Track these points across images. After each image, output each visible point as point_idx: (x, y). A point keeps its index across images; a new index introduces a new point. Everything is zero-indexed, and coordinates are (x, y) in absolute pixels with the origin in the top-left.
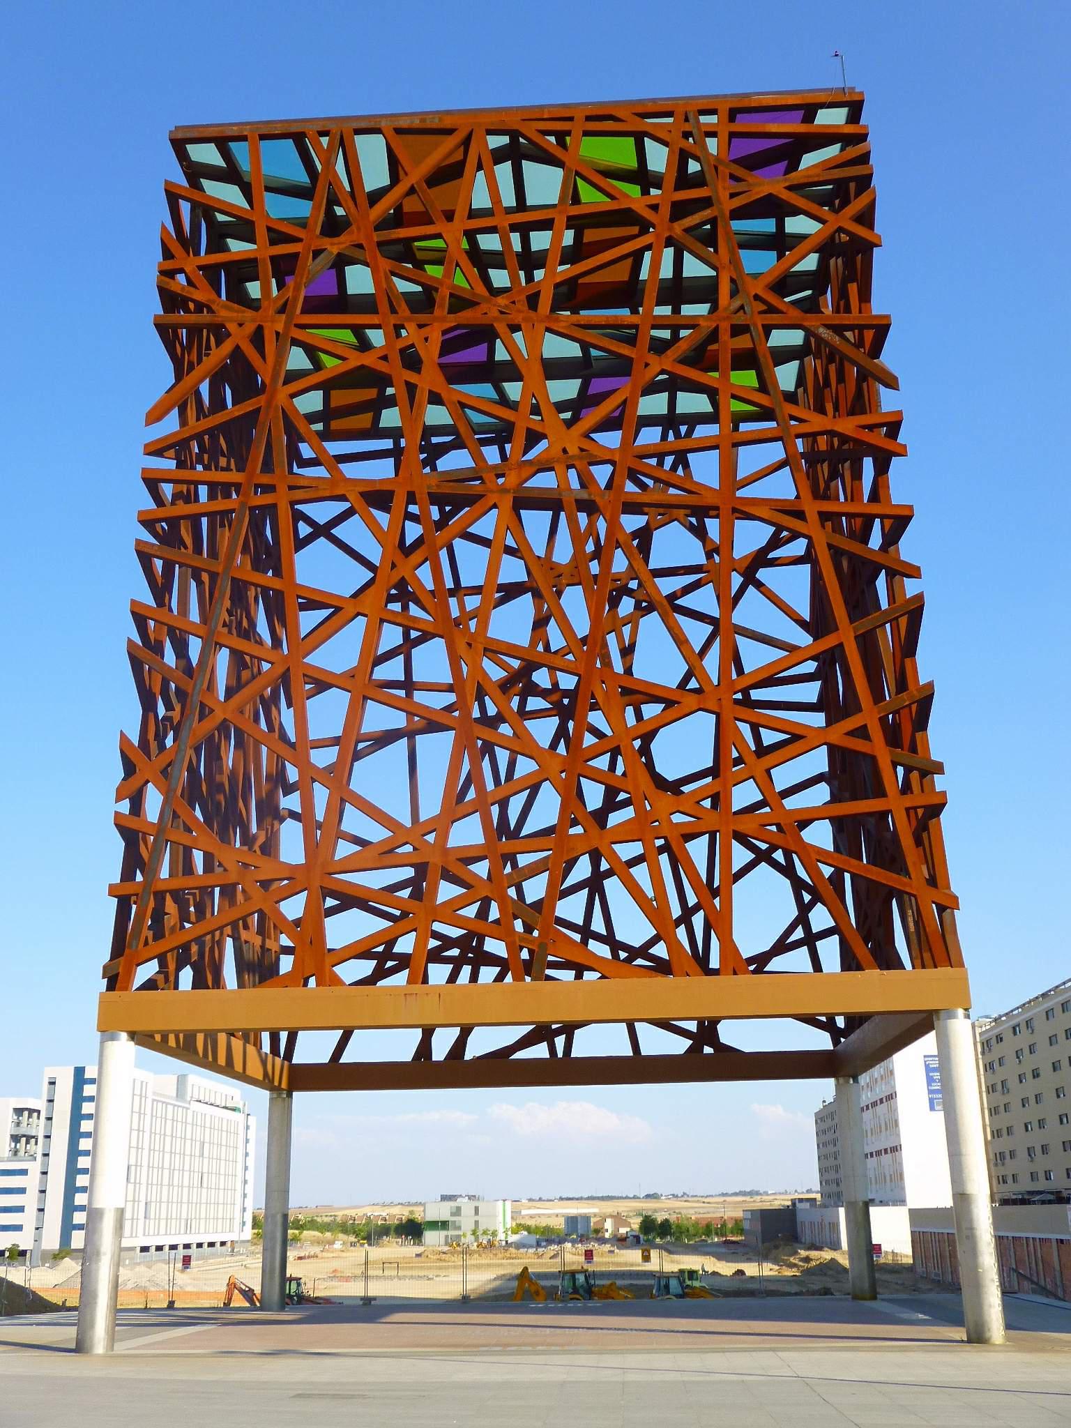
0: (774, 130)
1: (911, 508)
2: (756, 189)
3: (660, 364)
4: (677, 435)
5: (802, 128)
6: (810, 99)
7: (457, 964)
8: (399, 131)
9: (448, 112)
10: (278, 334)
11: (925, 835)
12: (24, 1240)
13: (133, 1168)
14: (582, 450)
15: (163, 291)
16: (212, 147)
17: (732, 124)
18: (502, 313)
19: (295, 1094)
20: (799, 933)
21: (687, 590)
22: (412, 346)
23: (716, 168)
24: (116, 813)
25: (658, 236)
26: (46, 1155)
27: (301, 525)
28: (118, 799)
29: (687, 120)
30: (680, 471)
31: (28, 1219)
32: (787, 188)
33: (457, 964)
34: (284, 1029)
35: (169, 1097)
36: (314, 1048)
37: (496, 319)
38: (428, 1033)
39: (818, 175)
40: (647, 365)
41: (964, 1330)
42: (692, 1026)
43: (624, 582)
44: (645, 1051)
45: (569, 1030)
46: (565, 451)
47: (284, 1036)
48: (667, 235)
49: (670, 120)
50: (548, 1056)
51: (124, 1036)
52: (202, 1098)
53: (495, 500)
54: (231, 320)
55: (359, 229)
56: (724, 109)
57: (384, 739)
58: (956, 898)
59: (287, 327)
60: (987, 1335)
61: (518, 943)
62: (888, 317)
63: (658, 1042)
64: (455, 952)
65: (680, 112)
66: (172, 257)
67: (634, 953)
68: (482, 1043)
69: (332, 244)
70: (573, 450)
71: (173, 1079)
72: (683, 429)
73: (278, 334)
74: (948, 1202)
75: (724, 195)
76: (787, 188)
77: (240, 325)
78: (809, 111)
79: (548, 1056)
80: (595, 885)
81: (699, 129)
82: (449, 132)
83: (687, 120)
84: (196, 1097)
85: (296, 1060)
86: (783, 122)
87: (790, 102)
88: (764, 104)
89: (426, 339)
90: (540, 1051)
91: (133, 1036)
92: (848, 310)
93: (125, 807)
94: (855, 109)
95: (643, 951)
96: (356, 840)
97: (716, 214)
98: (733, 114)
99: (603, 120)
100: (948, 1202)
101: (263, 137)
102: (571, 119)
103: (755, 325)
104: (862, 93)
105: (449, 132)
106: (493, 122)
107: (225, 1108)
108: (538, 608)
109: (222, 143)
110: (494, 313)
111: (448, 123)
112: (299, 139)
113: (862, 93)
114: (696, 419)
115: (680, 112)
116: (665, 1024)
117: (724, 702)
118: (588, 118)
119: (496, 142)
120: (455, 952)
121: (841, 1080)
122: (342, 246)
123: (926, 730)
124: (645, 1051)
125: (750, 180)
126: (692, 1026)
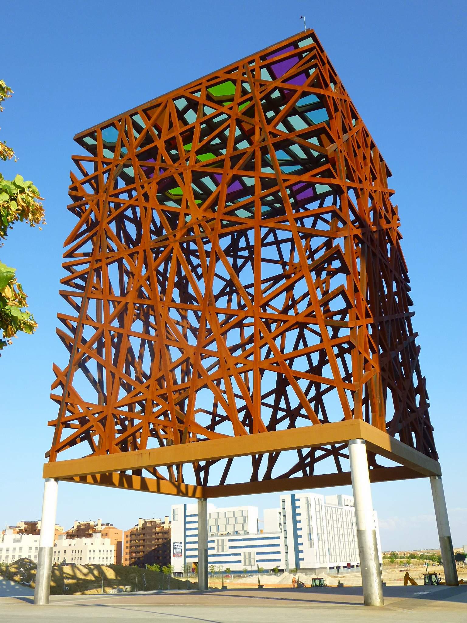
2: (269, 87)
9: (160, 97)
12: (282, 566)
13: (320, 535)
14: (204, 217)
19: (208, 499)
31: (282, 556)
32: (282, 82)
35: (336, 505)
37: (174, 173)
41: (362, 597)
46: (197, 219)
51: (52, 480)
52: (349, 504)
56: (257, 58)
59: (106, 198)
60: (369, 601)
70: (200, 218)
71: (336, 497)
76: (282, 82)
78: (295, 44)
82: (159, 105)
84: (347, 504)
85: (209, 484)
86: (280, 54)
91: (57, 479)
94: (312, 35)
98: (263, 58)
99: (214, 80)
101: (102, 129)
102: (201, 84)
105: (159, 105)
106: (173, 96)
111: (159, 101)
112: (113, 124)
118: (208, 81)
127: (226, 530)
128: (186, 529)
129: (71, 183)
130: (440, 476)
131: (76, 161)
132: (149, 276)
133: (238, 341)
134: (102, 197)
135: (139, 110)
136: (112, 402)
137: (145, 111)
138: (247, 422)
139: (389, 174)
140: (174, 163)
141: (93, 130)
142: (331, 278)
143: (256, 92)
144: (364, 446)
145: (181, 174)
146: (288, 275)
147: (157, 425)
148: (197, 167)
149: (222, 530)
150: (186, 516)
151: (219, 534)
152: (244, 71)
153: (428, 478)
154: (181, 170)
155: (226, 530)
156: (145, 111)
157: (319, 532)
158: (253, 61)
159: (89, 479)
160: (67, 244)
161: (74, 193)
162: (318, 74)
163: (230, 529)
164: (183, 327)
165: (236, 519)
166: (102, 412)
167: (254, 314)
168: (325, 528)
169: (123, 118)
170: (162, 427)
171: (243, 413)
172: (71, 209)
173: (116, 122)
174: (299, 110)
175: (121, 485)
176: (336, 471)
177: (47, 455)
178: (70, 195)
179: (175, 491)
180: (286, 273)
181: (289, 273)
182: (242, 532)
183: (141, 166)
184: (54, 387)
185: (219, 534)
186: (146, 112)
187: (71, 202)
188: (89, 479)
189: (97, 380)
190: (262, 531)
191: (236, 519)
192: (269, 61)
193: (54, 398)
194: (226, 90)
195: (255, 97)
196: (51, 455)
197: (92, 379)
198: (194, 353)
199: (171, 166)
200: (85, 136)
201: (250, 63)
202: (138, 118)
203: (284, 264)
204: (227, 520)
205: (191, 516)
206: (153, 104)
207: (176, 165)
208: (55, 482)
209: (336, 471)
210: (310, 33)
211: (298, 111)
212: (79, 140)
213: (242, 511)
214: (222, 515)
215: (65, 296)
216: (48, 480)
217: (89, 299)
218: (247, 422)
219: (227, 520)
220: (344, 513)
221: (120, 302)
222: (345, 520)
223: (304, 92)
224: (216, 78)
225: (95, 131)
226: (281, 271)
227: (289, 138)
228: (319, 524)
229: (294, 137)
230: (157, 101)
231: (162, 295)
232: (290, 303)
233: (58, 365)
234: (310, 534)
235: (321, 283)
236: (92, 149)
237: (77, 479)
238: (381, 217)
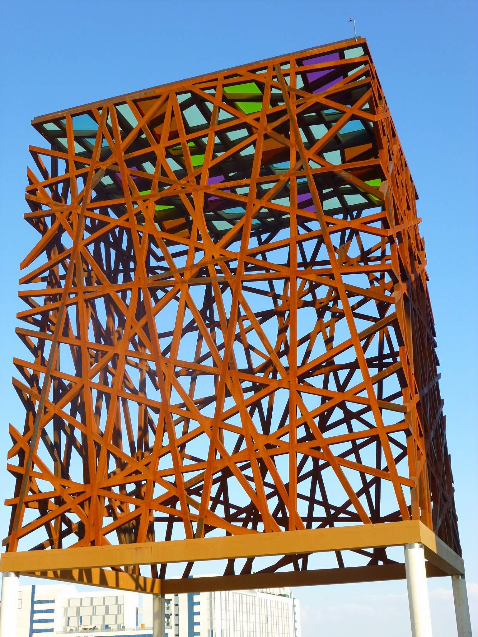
0: (319, 67)
3: (260, 204)
4: (352, 218)
5: (340, 62)
6: (338, 47)
7: (245, 522)
9: (157, 87)
10: (79, 215)
14: (221, 255)
15: (29, 201)
16: (52, 124)
18: (183, 188)
21: (360, 304)
22: (140, 212)
23: (289, 93)
24: (8, 464)
25: (259, 135)
26: (177, 625)
28: (9, 457)
29: (274, 70)
30: (169, 289)
32: (325, 97)
33: (245, 522)
34: (159, 563)
36: (175, 572)
37: (180, 192)
38: (231, 562)
39: (342, 88)
40: (254, 205)
42: (371, 551)
43: (325, 303)
44: (346, 565)
45: (305, 556)
46: (213, 257)
47: (159, 567)
48: (264, 133)
49: (266, 71)
50: (338, 567)
51: (13, 574)
53: (179, 287)
54: (58, 211)
55: (115, 155)
56: (293, 60)
59: (83, 211)
61: (189, 519)
63: (354, 560)
64: (244, 516)
65: (270, 66)
66: (33, 184)
67: (339, 510)
68: (260, 565)
69: (103, 165)
70: (217, 256)
72: (355, 213)
73: (79, 215)
75: (293, 106)
76: (325, 97)
77: (62, 213)
78: (341, 53)
79: (338, 567)
80: (316, 475)
81: (280, 73)
82: (158, 97)
83: (274, 70)
85: (167, 577)
87: (327, 50)
88: (314, 53)
89: (147, 207)
90: (289, 568)
91: (17, 574)
93: (15, 461)
94: (365, 46)
95: (343, 509)
96: (193, 458)
97: (289, 117)
98: (299, 62)
101: (72, 116)
102: (216, 80)
104: (365, 39)
105: (158, 97)
106: (176, 88)
107: (281, 595)
108: (280, 322)
109: (57, 121)
110: (179, 188)
111: (157, 92)
112: (90, 113)
113: (365, 39)
114: (360, 208)
115: (270, 66)
116: (359, 551)
117: (291, 383)
118: (226, 78)
119: (182, 98)
120: (244, 516)
121: (454, 577)
122: (108, 165)
124: (346, 565)
125: (306, 97)
126: (371, 551)
127: (91, 624)
128: (32, 621)
129: (28, 185)
130: (463, 576)
131: (35, 153)
132: (147, 323)
134: (76, 209)
135: (127, 99)
136: (97, 481)
137: (135, 102)
139: (417, 198)
140: (179, 179)
141: (60, 115)
142: (336, 322)
143: (291, 104)
144: (422, 550)
146: (280, 312)
147: (113, 500)
148: (212, 189)
149: (86, 623)
150: (33, 602)
151: (81, 629)
152: (274, 73)
153: (450, 577)
154: (189, 189)
155: (91, 624)
156: (135, 102)
157: (224, 628)
158: (288, 63)
159: (50, 574)
160: (24, 265)
161: (33, 198)
162: (371, 96)
163: (97, 621)
164: (141, 370)
165: (107, 608)
167: (290, 386)
168: (232, 622)
169: (105, 106)
170: (118, 503)
171: (217, 485)
172: (29, 219)
173: (94, 110)
174: (327, 118)
175: (81, 581)
176: (337, 566)
177: (6, 543)
178: (27, 200)
179: (133, 585)
180: (279, 310)
181: (282, 310)
182: (114, 627)
183: (131, 175)
184: (10, 455)
185: (81, 629)
186: (137, 103)
187: (29, 210)
188: (50, 574)
190: (142, 626)
191: (107, 608)
192: (306, 67)
193: (10, 469)
195: (290, 111)
196: (10, 544)
199: (175, 182)
201: (282, 64)
202: (126, 111)
203: (276, 297)
204: (94, 609)
205: (40, 602)
206: (149, 95)
207: (183, 182)
208: (17, 577)
209: (337, 566)
210: (362, 42)
211: (324, 119)
212: (38, 126)
213: (117, 597)
214: (86, 602)
215: (23, 335)
216: (7, 575)
217: (59, 343)
219: (94, 609)
220: (257, 603)
221: (106, 352)
222: (257, 612)
223: (353, 115)
224: (236, 75)
226: (271, 307)
227: (335, 170)
228: (224, 618)
229: (341, 171)
230: (154, 92)
231: (120, 329)
232: (283, 348)
234: (212, 631)
235: (324, 327)
236: (51, 137)
237: (38, 573)
238: (415, 260)
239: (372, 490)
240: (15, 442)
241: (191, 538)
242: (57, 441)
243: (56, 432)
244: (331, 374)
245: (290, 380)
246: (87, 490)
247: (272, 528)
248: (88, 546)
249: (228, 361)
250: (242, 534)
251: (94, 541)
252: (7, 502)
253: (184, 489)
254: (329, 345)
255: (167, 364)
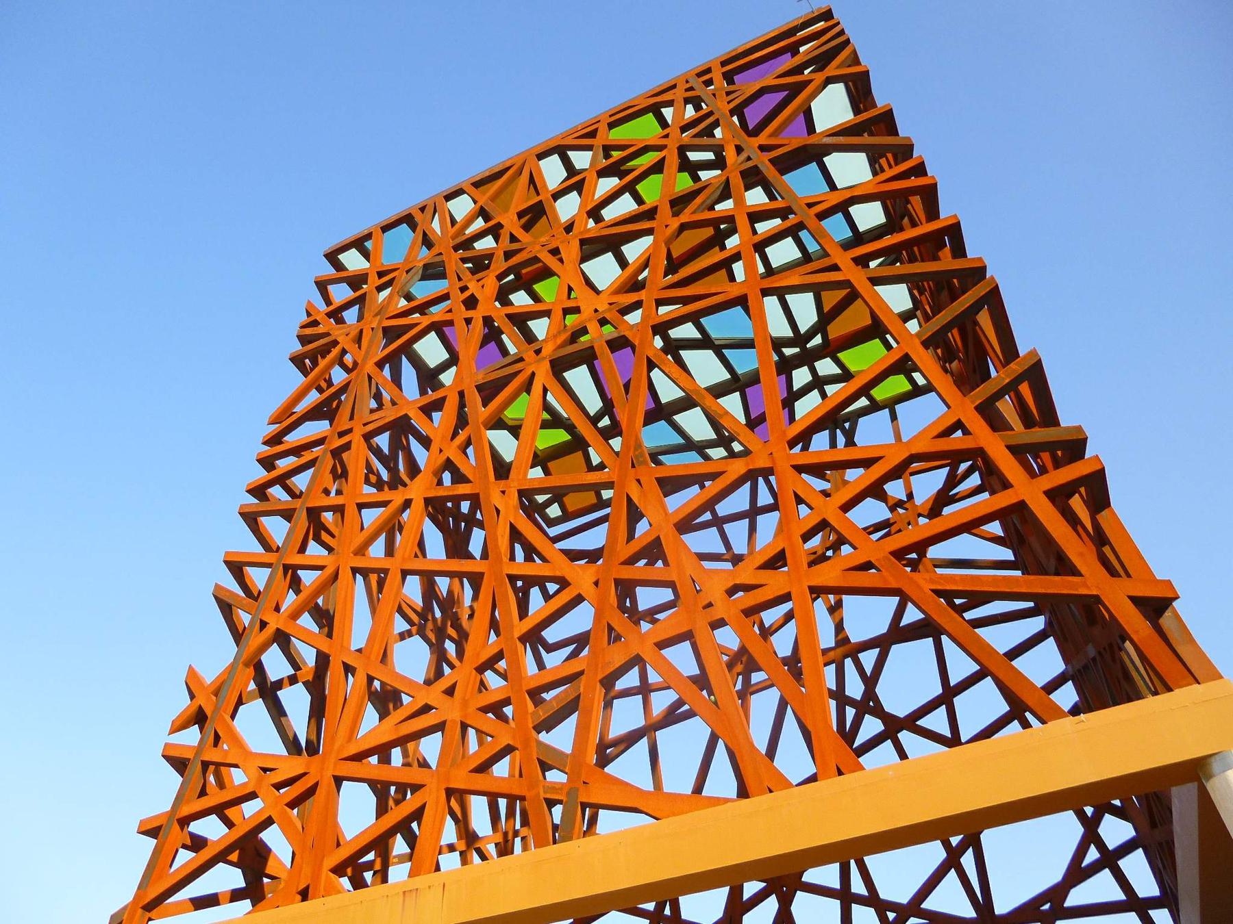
1: (955, 216)
8: (477, 184)
11: (1107, 550)
17: (921, 349)
20: (1093, 854)
27: (556, 587)
43: (820, 552)
46: (596, 311)
57: (630, 740)
58: (1168, 583)
61: (542, 795)
62: (955, 216)
74: (698, 672)
92: (883, 170)
94: (827, 15)
100: (698, 672)
103: (763, 162)
111: (508, 165)
123: (1108, 505)
133: (639, 722)
138: (914, 556)
145: (555, 252)
166: (304, 774)
172: (297, 360)
184: (179, 726)
187: (297, 347)
189: (303, 744)
194: (644, 129)
197: (291, 736)
198: (596, 583)
200: (344, 248)
215: (251, 519)
218: (914, 556)
225: (369, 236)
233: (199, 670)
239: (968, 860)
240: (192, 696)
241: (547, 844)
242: (314, 738)
243: (313, 720)
244: (848, 662)
245: (774, 451)
246: (312, 771)
247: (766, 784)
248: (293, 902)
249: (631, 454)
250: (682, 813)
251: (307, 888)
252: (152, 830)
253: (531, 725)
254: (836, 614)
255: (503, 492)
